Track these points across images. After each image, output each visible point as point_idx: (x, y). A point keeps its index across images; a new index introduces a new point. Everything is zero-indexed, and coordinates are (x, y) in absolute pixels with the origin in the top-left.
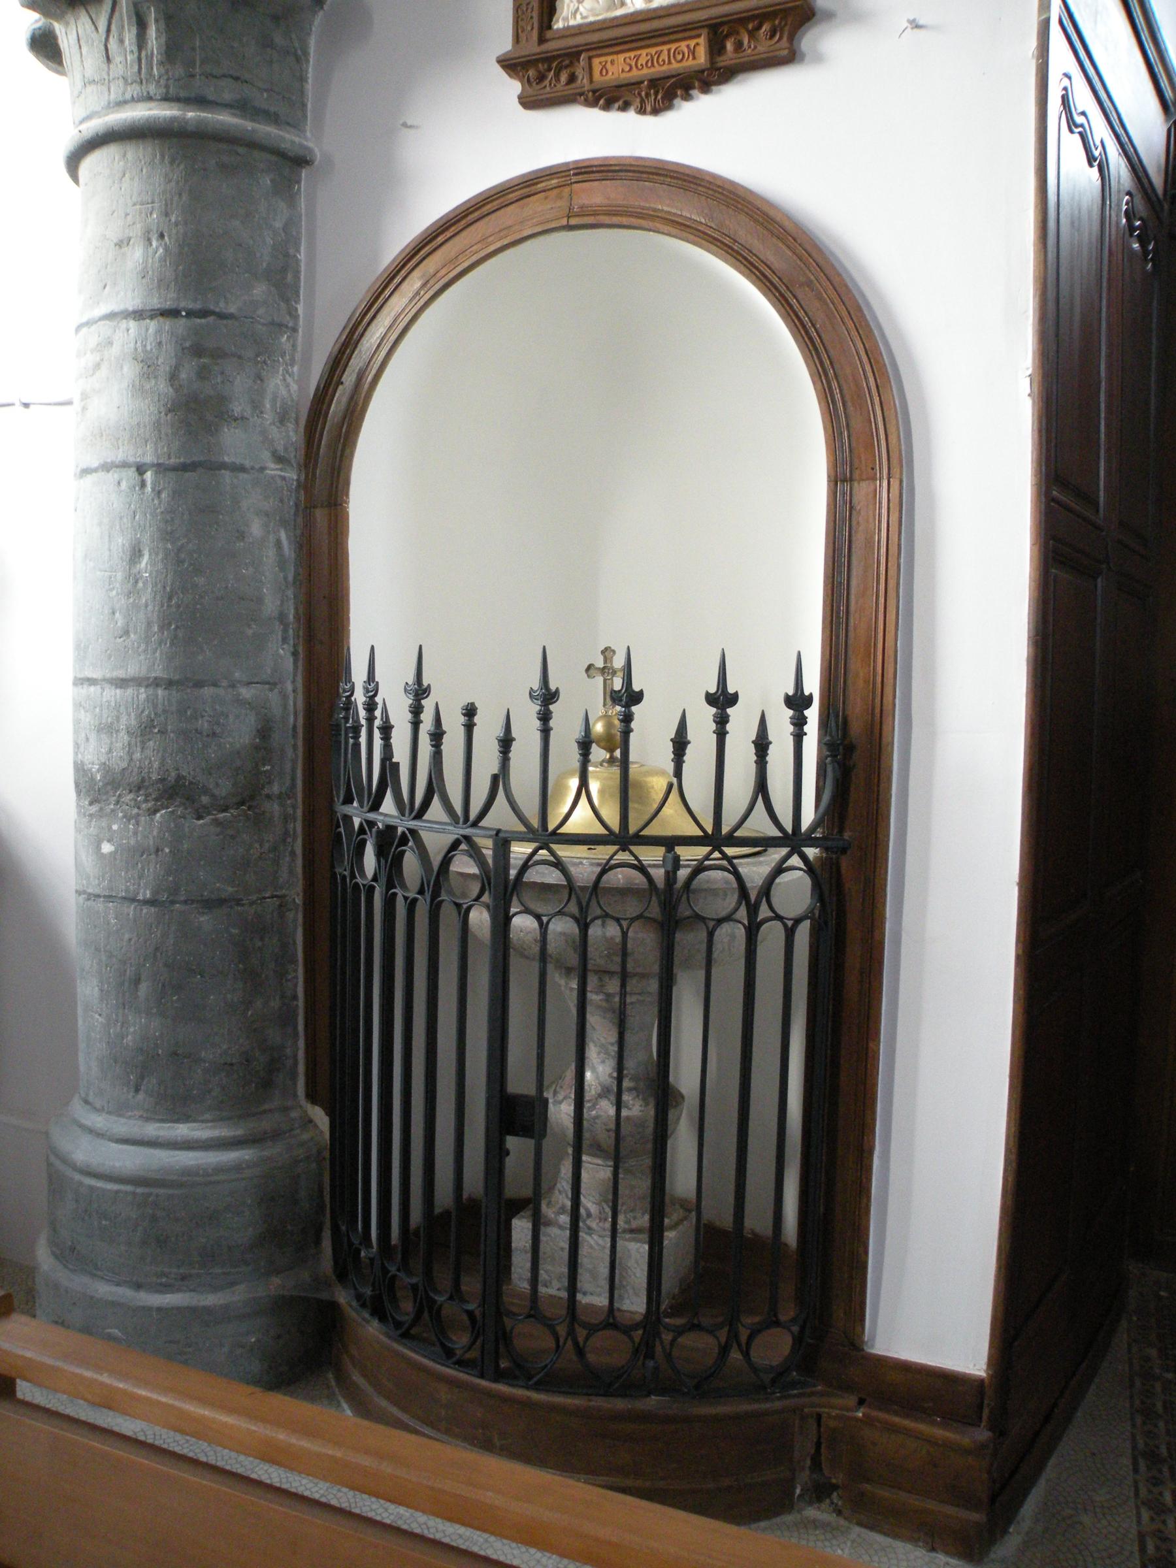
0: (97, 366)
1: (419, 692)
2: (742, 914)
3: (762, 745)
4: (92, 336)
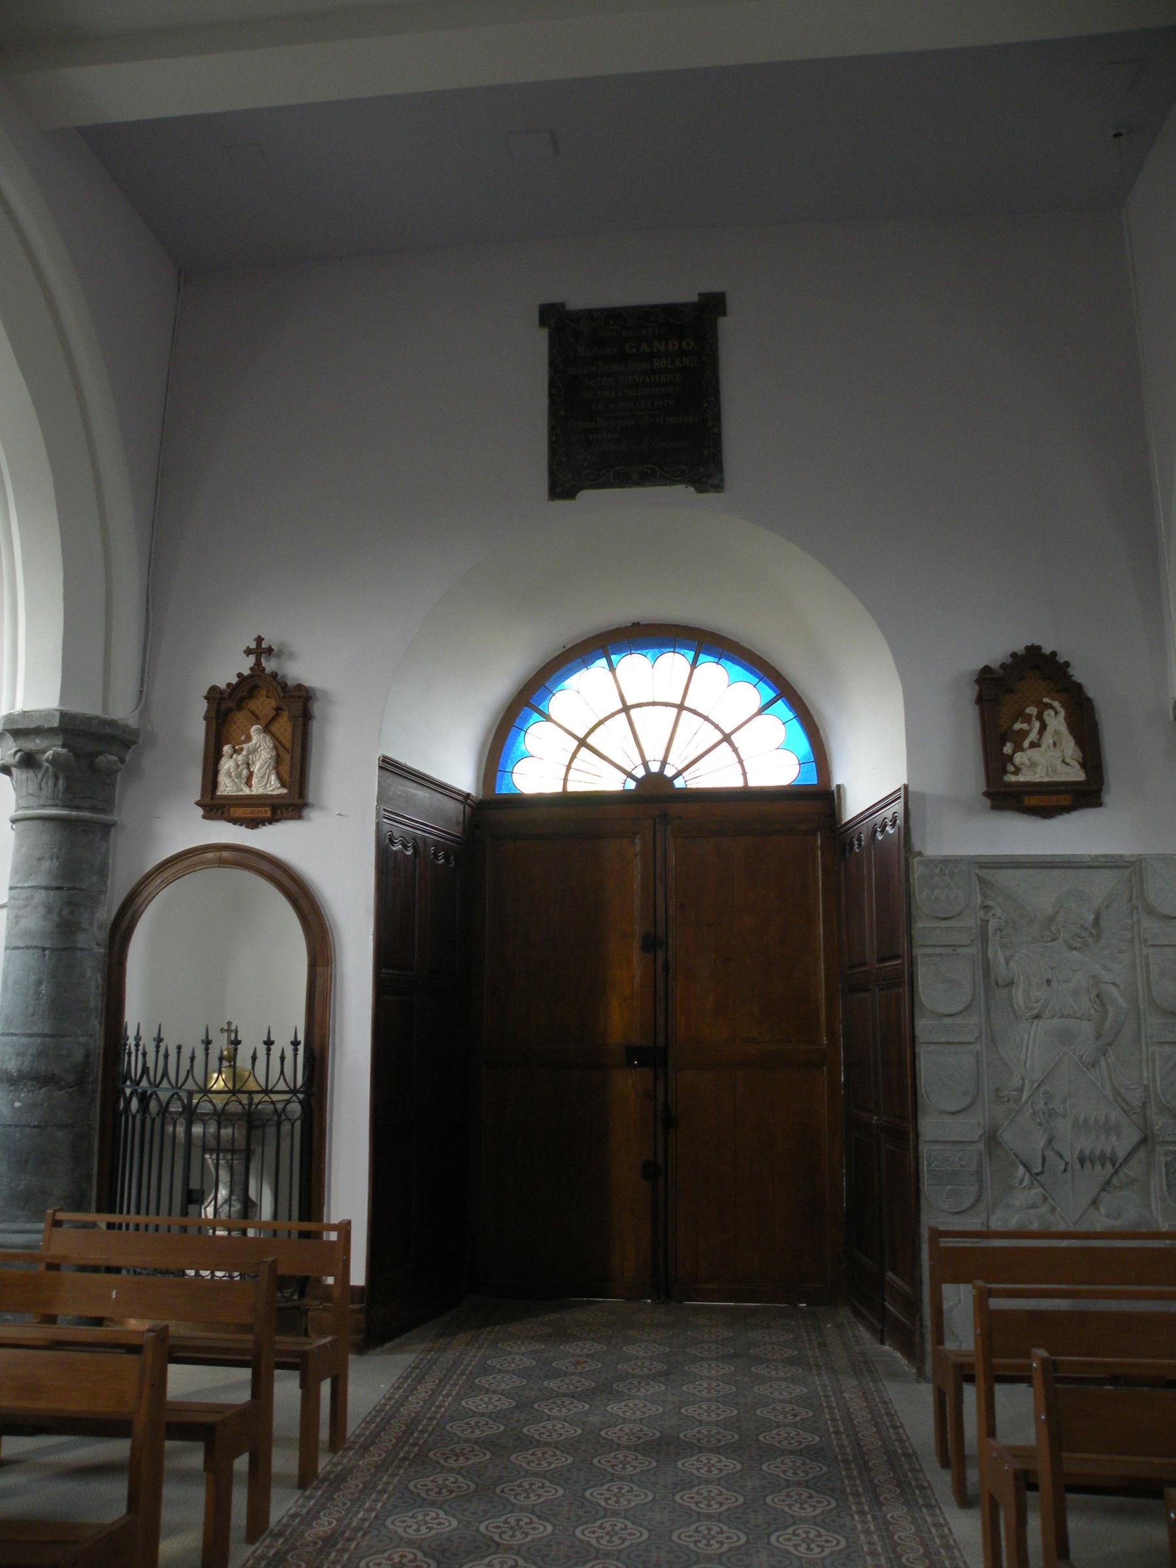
0: (25, 906)
1: (159, 1040)
2: (275, 1118)
3: (282, 1058)
4: (25, 894)
